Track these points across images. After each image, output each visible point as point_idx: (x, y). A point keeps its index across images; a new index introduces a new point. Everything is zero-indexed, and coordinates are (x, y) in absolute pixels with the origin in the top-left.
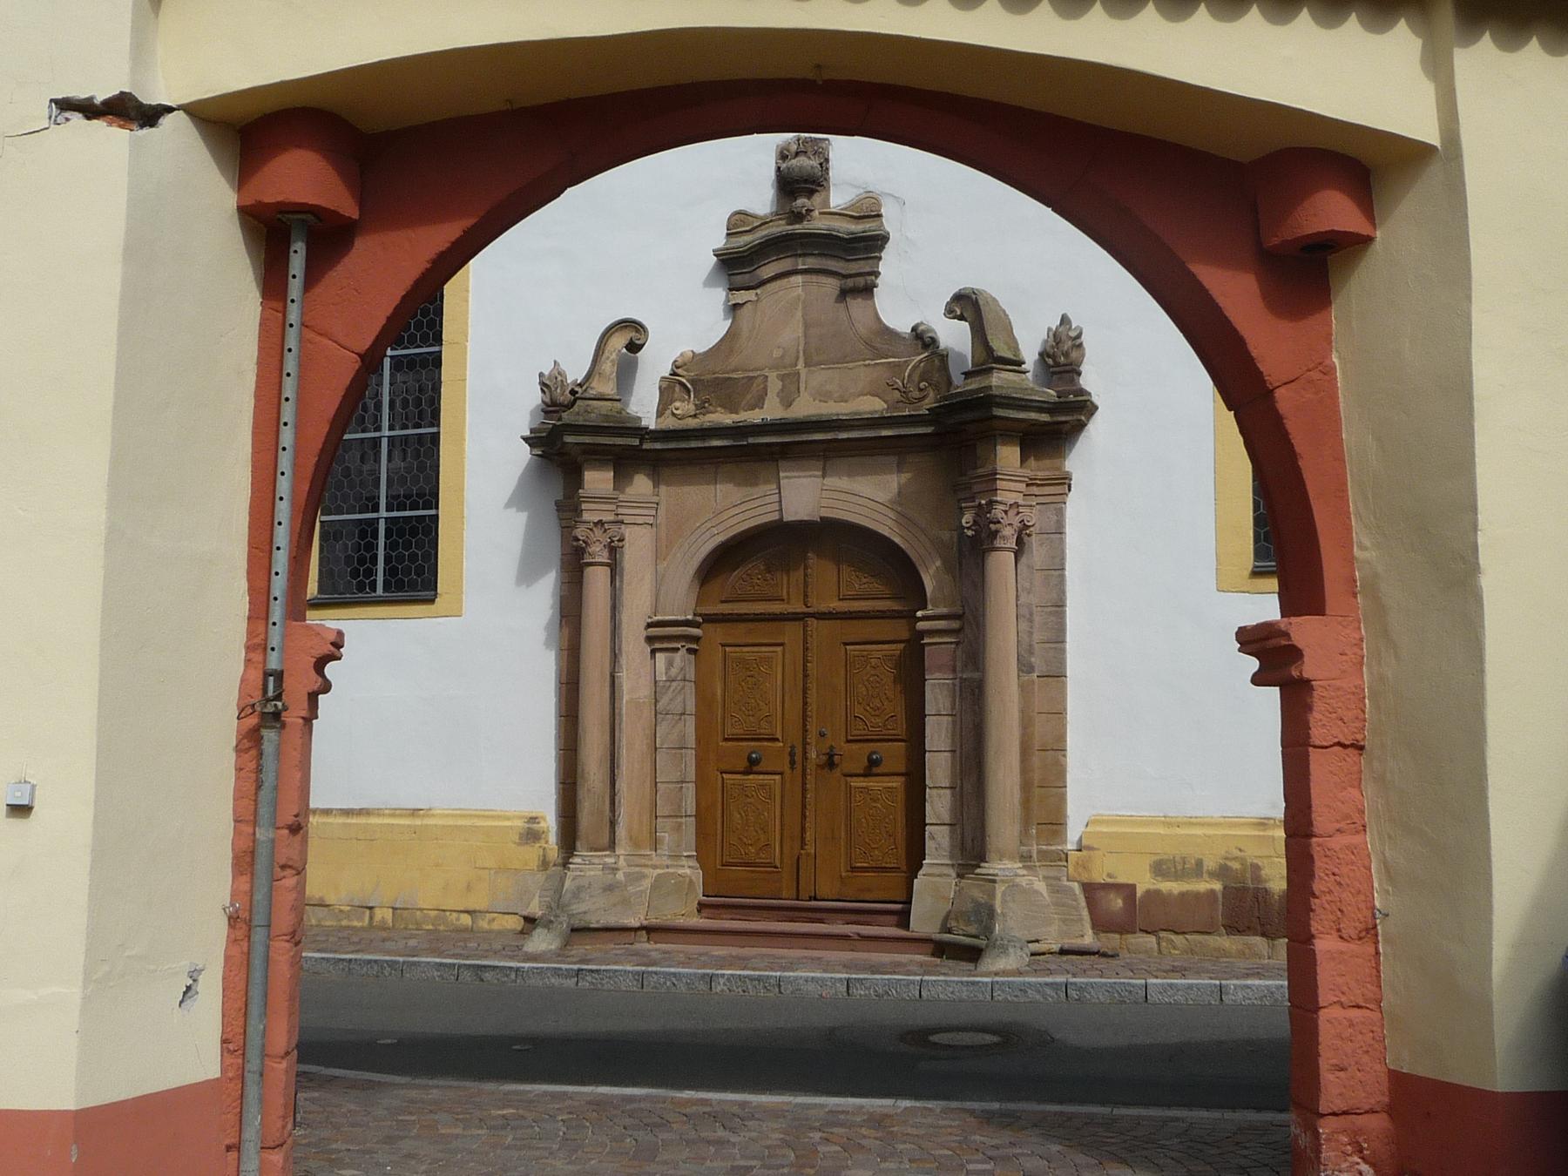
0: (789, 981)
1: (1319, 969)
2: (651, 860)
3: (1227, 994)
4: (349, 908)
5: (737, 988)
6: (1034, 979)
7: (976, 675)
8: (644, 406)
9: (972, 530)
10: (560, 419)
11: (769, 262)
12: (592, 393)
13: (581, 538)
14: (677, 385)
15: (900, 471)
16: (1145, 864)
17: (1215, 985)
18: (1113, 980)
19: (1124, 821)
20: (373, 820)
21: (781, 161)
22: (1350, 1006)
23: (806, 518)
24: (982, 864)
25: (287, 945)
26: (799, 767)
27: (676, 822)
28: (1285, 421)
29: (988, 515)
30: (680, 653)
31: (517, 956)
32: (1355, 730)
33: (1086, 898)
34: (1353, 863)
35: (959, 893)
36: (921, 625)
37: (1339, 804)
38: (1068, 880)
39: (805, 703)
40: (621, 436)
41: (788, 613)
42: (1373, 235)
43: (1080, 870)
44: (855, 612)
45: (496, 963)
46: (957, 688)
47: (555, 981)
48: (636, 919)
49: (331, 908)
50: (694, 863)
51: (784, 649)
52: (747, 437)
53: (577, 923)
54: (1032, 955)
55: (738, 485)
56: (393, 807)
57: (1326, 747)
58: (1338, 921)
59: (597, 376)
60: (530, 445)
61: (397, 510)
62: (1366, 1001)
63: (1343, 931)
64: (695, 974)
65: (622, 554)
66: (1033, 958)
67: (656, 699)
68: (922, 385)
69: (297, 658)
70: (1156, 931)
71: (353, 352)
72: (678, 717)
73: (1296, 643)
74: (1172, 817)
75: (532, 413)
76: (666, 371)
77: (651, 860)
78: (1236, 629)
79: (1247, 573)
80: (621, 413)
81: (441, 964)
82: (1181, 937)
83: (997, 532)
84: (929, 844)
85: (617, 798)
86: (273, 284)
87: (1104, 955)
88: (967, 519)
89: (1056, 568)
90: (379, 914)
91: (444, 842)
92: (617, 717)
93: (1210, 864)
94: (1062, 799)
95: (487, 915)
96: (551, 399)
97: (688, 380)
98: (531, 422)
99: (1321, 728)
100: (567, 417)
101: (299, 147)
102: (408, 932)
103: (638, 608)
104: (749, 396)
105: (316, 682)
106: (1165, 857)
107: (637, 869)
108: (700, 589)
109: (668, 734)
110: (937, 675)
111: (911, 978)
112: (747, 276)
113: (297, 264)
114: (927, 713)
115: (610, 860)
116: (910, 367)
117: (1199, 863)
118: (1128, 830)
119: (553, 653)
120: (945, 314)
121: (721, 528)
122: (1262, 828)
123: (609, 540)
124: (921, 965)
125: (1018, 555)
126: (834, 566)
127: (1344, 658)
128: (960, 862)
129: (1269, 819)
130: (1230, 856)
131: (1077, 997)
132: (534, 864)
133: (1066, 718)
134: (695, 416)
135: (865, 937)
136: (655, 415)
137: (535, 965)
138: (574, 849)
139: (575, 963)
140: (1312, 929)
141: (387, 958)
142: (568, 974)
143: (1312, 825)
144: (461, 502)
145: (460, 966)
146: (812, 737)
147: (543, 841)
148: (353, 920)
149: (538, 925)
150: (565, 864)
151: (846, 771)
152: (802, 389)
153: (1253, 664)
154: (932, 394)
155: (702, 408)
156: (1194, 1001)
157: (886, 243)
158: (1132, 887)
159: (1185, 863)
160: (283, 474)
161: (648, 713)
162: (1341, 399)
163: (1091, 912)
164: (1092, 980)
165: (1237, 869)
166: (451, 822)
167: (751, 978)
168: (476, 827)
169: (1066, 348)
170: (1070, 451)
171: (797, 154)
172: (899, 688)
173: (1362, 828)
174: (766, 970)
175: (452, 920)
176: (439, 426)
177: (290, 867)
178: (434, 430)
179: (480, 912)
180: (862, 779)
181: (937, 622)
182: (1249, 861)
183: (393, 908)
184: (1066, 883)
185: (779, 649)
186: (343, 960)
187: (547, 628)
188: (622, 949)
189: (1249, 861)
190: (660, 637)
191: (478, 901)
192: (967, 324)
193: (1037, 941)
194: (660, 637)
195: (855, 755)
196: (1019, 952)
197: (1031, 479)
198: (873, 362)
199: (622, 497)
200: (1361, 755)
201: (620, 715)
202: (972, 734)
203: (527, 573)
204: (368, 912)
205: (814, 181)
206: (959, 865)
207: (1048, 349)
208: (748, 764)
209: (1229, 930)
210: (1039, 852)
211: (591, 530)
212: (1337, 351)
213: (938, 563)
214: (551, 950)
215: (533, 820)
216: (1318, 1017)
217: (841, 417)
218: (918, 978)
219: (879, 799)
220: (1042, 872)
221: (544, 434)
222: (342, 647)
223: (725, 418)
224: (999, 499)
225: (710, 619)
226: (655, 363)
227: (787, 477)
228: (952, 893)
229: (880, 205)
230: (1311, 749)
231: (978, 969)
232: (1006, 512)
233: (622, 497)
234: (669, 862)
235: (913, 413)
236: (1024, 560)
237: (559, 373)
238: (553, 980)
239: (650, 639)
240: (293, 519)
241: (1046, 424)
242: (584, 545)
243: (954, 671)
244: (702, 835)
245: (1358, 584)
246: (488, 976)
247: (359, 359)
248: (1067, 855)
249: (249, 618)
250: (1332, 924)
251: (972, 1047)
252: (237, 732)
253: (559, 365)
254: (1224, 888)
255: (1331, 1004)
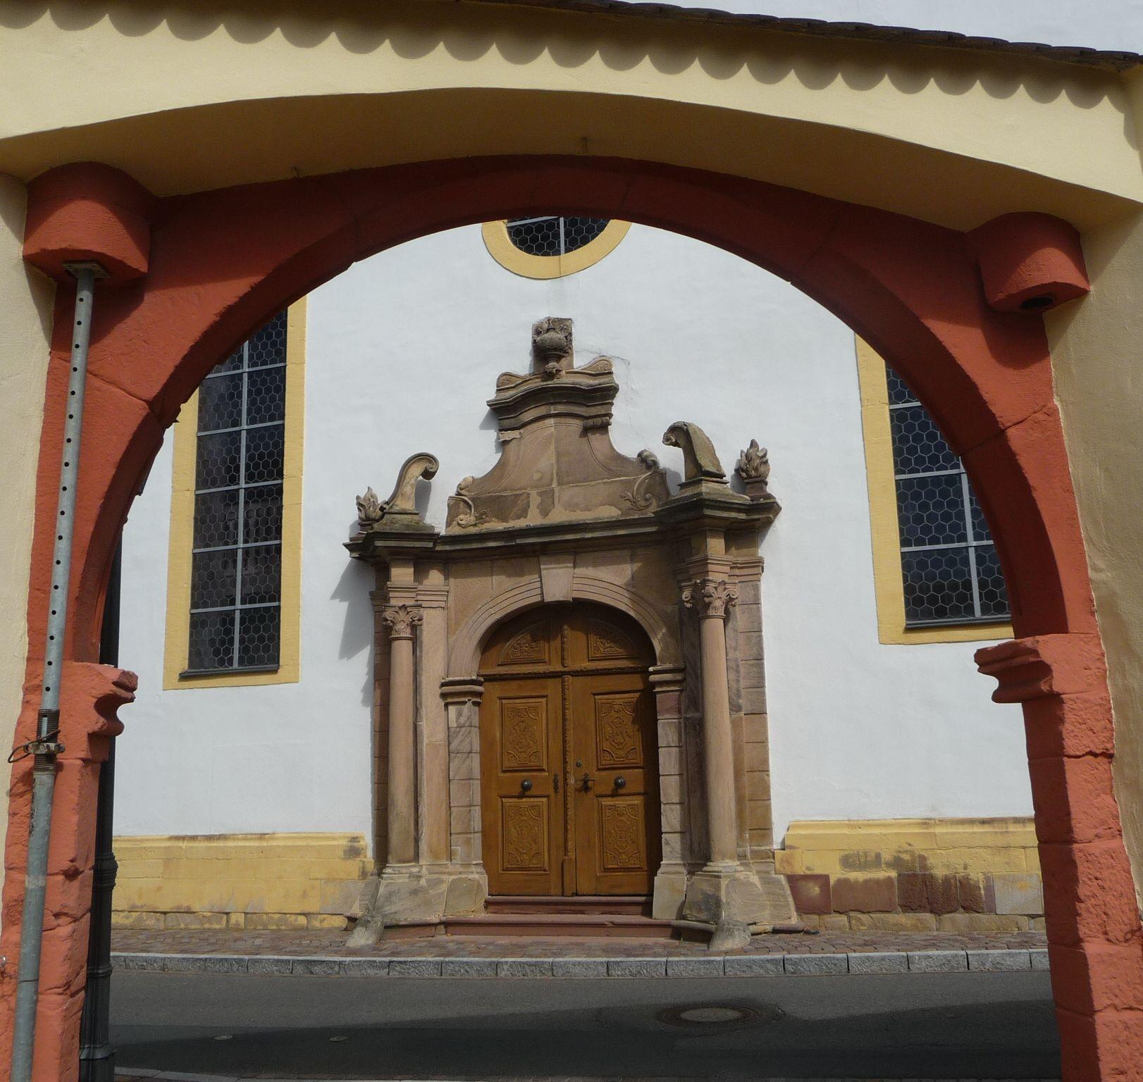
0: (560, 965)
1: (1091, 973)
2: (447, 868)
3: (913, 963)
4: (210, 914)
5: (518, 972)
6: (758, 957)
7: (697, 715)
8: (437, 518)
9: (691, 603)
10: (372, 529)
11: (529, 410)
12: (396, 509)
13: (389, 619)
14: (462, 503)
15: (632, 560)
16: (836, 857)
17: (903, 956)
18: (821, 955)
19: (818, 825)
20: (230, 844)
21: (536, 336)
22: (1123, 1009)
23: (561, 599)
24: (708, 864)
25: (60, 998)
26: (561, 790)
27: (467, 838)
28: (1018, 457)
29: (703, 591)
30: (467, 706)
31: (341, 951)
32: (1105, 740)
33: (790, 886)
34: (1113, 867)
35: (691, 887)
36: (653, 678)
37: (1096, 810)
38: (776, 874)
39: (564, 742)
40: (684, 760)
41: (550, 672)
42: (1088, 289)
43: (785, 865)
44: (601, 670)
45: (323, 958)
46: (682, 725)
47: (371, 972)
48: (437, 916)
49: (196, 914)
50: (481, 869)
51: (547, 700)
52: (515, 539)
53: (389, 922)
54: (752, 935)
55: (509, 576)
56: (246, 832)
57: (1079, 757)
58: (1104, 924)
59: (400, 497)
60: (350, 550)
61: (249, 604)
62: (1138, 1002)
63: (1109, 933)
64: (484, 962)
65: (421, 631)
66: (753, 937)
67: (449, 741)
68: (647, 496)
69: (77, 699)
70: (846, 912)
71: (141, 399)
72: (466, 755)
73: (1042, 659)
74: (854, 821)
75: (352, 527)
76: (453, 493)
77: (447, 868)
78: (975, 652)
79: (901, 629)
80: (418, 523)
81: (278, 961)
82: (866, 915)
83: (710, 603)
84: (665, 849)
85: (420, 819)
86: (60, 338)
87: (807, 933)
88: (686, 594)
89: (755, 631)
90: (234, 918)
91: (285, 859)
92: (419, 757)
93: (887, 856)
94: (768, 810)
95: (319, 916)
96: (366, 515)
97: (469, 499)
98: (350, 534)
99: (1075, 737)
100: (377, 527)
101: (84, 198)
102: (258, 932)
103: (434, 671)
104: (515, 510)
105: (97, 723)
106: (851, 852)
107: (436, 876)
108: (482, 654)
109: (459, 768)
110: (667, 716)
111: (658, 959)
112: (513, 420)
113: (83, 311)
114: (659, 745)
115: (415, 870)
116: (638, 483)
117: (878, 856)
118: (820, 832)
119: (369, 709)
120: (663, 442)
121: (496, 609)
122: (925, 826)
123: (411, 620)
124: (665, 946)
125: (726, 621)
126: (584, 635)
127: (1088, 672)
128: (689, 862)
129: (930, 819)
130: (901, 849)
131: (793, 971)
132: (356, 874)
133: (768, 745)
134: (475, 525)
135: (615, 924)
136: (445, 525)
137: (355, 959)
138: (387, 862)
139: (386, 956)
140: (1080, 933)
141: (235, 957)
142: (382, 965)
143: (1072, 831)
144: (298, 595)
145: (294, 962)
146: (571, 767)
147: (362, 856)
148: (212, 924)
149: (357, 924)
150: (380, 874)
151: (598, 793)
152: (556, 502)
153: (993, 683)
154: (655, 504)
155: (480, 519)
156: (886, 970)
157: (617, 392)
158: (826, 878)
159: (866, 857)
160: (63, 513)
161: (443, 752)
162: (1065, 438)
163: (795, 899)
164: (804, 956)
165: (908, 860)
166: (290, 843)
167: (529, 964)
168: (310, 846)
169: (756, 465)
170: (762, 541)
171: (548, 330)
172: (637, 727)
173: (1118, 833)
174: (541, 957)
175: (291, 921)
176: (281, 539)
177: (65, 914)
178: (277, 542)
179: (314, 914)
180: (610, 799)
181: (662, 675)
182: (917, 853)
183: (245, 913)
184: (774, 876)
185: (544, 700)
186: (200, 959)
187: (365, 690)
188: (426, 941)
189: (917, 853)
190: (452, 693)
191: (312, 905)
192: (681, 449)
193: (755, 924)
194: (452, 693)
195: (604, 781)
196: (743, 934)
197: (734, 563)
198: (609, 481)
199: (420, 587)
200: (1110, 763)
201: (422, 754)
202: (696, 760)
203: (348, 649)
204: (225, 917)
205: (561, 349)
206: (689, 864)
207: (742, 466)
208: (521, 790)
209: (904, 908)
210: (752, 852)
211: (397, 612)
212: (1058, 395)
213: (664, 631)
214: (368, 945)
215: (355, 839)
216: (1094, 1020)
217: (586, 521)
218: (664, 959)
219: (624, 814)
220: (755, 868)
221: (360, 542)
222: (135, 689)
223: (499, 526)
224: (710, 578)
225: (490, 679)
226: (444, 487)
227: (545, 569)
228: (685, 887)
229: (611, 366)
230: (1065, 759)
231: (711, 949)
232: (716, 588)
233: (420, 587)
234: (461, 870)
235: (642, 516)
236: (730, 625)
237: (372, 496)
238: (369, 971)
239: (444, 696)
240: (73, 557)
241: (743, 521)
242: (391, 624)
243: (680, 712)
244: (487, 846)
245: (1095, 604)
246: (316, 969)
247: (147, 406)
248: (774, 854)
249: (29, 659)
250: (1098, 927)
251: (718, 1023)
252: (12, 775)
253: (371, 490)
254: (899, 875)
255: (1105, 1008)
